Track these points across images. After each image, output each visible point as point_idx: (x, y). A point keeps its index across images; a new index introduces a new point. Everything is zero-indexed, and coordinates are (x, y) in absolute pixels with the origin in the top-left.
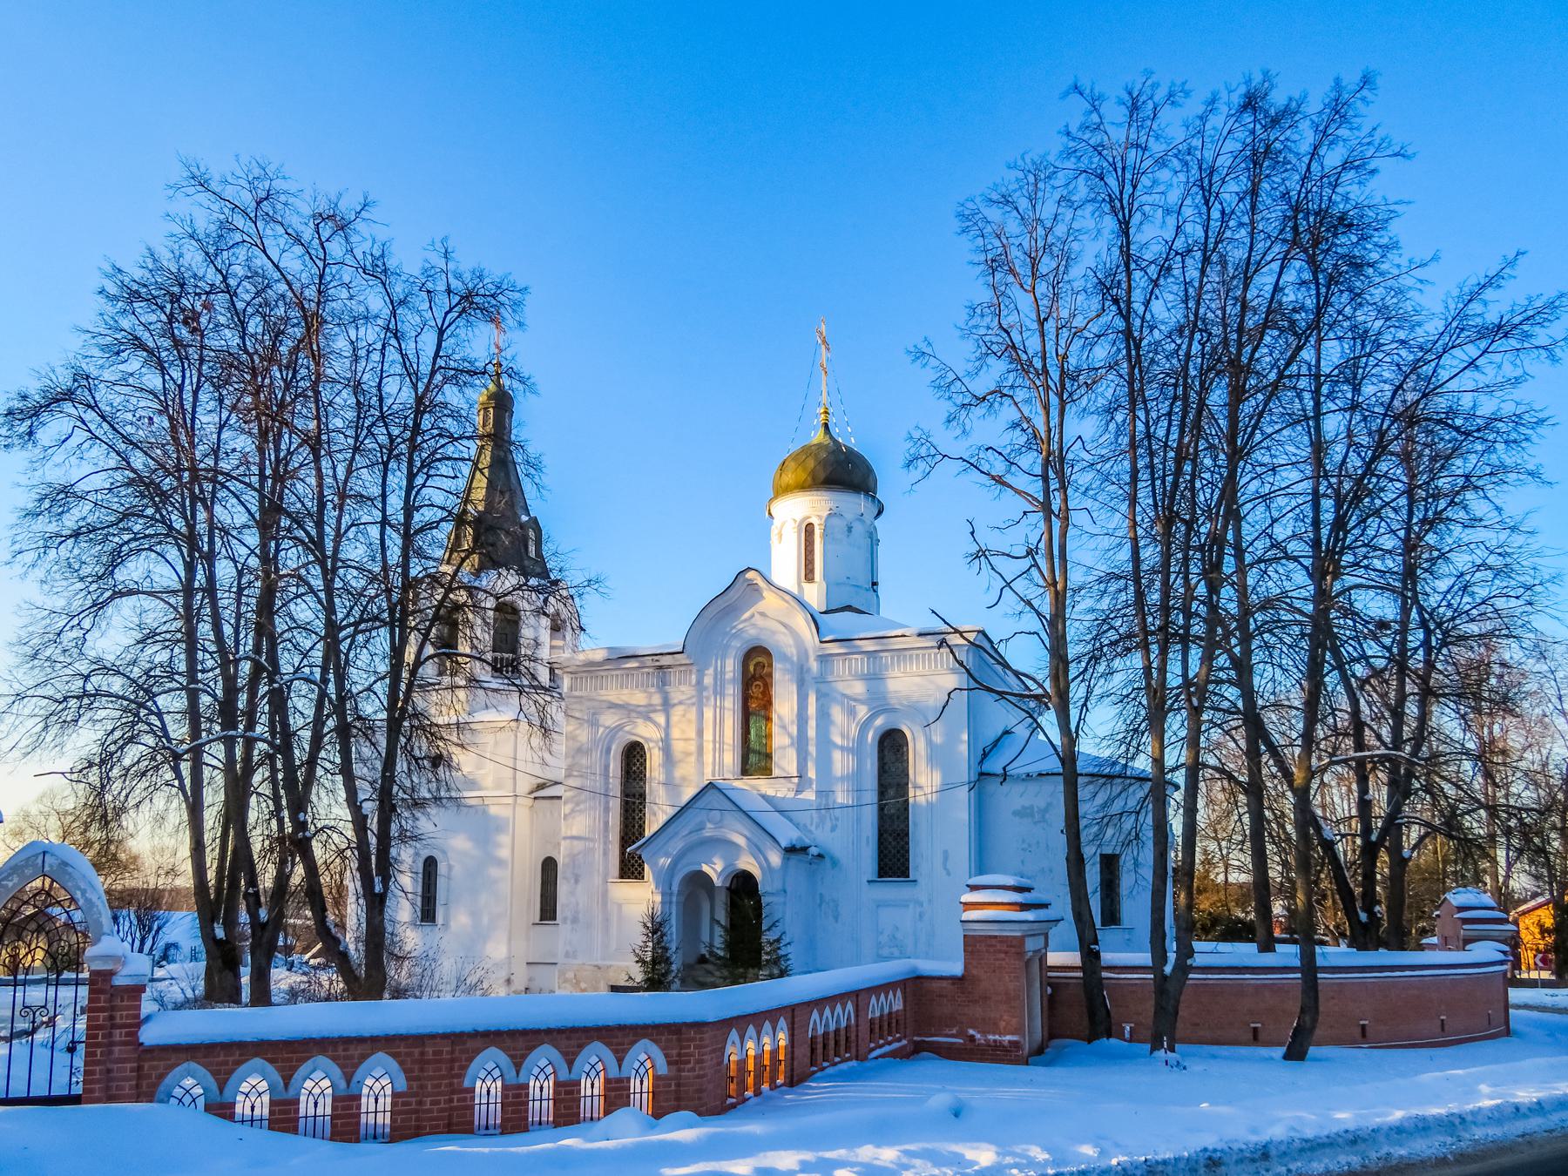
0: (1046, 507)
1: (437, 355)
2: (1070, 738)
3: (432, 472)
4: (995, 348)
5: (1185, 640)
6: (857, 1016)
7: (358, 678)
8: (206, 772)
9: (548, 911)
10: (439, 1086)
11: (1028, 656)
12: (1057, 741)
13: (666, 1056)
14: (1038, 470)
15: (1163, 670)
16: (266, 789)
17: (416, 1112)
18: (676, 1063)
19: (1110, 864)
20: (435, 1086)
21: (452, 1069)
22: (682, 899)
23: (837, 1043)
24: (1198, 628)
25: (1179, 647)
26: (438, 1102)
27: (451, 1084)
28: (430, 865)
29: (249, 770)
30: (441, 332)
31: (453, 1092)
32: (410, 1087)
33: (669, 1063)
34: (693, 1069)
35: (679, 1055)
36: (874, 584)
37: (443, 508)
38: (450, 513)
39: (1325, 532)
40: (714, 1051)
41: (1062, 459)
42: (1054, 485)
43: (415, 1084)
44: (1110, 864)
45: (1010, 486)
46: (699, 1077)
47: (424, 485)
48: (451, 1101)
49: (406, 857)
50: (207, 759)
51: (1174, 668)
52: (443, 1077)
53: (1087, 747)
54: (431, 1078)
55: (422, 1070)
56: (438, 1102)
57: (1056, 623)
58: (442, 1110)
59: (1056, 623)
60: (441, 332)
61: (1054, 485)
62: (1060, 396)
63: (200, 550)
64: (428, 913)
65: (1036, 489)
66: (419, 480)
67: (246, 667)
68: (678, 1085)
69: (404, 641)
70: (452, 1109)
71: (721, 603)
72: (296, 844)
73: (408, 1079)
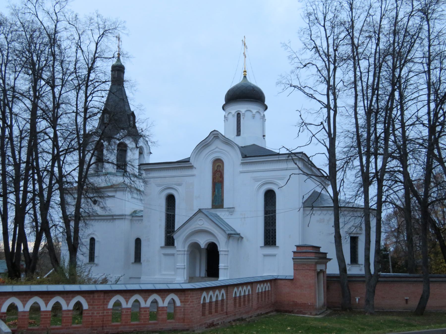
0: (328, 106)
1: (96, 53)
2: (336, 193)
3: (93, 96)
4: (309, 47)
5: (376, 155)
6: (252, 291)
7: (67, 169)
8: (9, 206)
9: (138, 258)
10: (99, 308)
11: (321, 162)
12: (332, 195)
13: (180, 299)
14: (325, 92)
15: (368, 167)
16: (31, 212)
17: (91, 316)
18: (183, 302)
19: (354, 240)
20: (98, 308)
21: (104, 302)
22: (189, 253)
23: (244, 301)
24: (381, 151)
25: (373, 157)
26: (99, 313)
27: (104, 307)
28: (92, 241)
29: (25, 204)
30: (97, 44)
31: (104, 310)
32: (89, 308)
33: (181, 302)
34: (190, 304)
35: (185, 299)
36: (264, 136)
37: (98, 108)
38: (101, 110)
39: (432, 115)
40: (197, 299)
41: (335, 89)
42: (331, 97)
43: (91, 307)
44: (354, 240)
45: (315, 98)
46: (191, 307)
47: (91, 101)
48: (103, 313)
49: (85, 240)
50: (9, 200)
51: (372, 165)
52: (101, 305)
53: (341, 197)
54: (97, 305)
55: (93, 302)
56: (99, 313)
57: (331, 150)
58: (100, 316)
59: (331, 150)
60: (97, 44)
61: (331, 97)
62: (334, 64)
63: (7, 124)
64: (92, 258)
65: (324, 99)
66: (89, 99)
67: (23, 166)
68: (184, 310)
69: (84, 156)
70: (104, 316)
71: (204, 142)
72: (43, 229)
73: (89, 305)
